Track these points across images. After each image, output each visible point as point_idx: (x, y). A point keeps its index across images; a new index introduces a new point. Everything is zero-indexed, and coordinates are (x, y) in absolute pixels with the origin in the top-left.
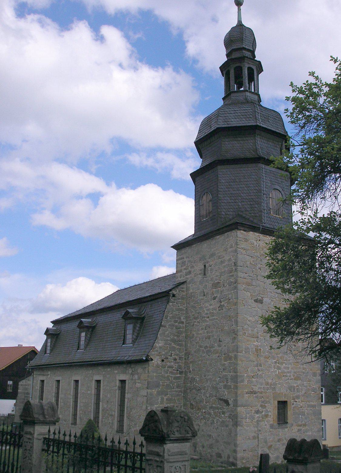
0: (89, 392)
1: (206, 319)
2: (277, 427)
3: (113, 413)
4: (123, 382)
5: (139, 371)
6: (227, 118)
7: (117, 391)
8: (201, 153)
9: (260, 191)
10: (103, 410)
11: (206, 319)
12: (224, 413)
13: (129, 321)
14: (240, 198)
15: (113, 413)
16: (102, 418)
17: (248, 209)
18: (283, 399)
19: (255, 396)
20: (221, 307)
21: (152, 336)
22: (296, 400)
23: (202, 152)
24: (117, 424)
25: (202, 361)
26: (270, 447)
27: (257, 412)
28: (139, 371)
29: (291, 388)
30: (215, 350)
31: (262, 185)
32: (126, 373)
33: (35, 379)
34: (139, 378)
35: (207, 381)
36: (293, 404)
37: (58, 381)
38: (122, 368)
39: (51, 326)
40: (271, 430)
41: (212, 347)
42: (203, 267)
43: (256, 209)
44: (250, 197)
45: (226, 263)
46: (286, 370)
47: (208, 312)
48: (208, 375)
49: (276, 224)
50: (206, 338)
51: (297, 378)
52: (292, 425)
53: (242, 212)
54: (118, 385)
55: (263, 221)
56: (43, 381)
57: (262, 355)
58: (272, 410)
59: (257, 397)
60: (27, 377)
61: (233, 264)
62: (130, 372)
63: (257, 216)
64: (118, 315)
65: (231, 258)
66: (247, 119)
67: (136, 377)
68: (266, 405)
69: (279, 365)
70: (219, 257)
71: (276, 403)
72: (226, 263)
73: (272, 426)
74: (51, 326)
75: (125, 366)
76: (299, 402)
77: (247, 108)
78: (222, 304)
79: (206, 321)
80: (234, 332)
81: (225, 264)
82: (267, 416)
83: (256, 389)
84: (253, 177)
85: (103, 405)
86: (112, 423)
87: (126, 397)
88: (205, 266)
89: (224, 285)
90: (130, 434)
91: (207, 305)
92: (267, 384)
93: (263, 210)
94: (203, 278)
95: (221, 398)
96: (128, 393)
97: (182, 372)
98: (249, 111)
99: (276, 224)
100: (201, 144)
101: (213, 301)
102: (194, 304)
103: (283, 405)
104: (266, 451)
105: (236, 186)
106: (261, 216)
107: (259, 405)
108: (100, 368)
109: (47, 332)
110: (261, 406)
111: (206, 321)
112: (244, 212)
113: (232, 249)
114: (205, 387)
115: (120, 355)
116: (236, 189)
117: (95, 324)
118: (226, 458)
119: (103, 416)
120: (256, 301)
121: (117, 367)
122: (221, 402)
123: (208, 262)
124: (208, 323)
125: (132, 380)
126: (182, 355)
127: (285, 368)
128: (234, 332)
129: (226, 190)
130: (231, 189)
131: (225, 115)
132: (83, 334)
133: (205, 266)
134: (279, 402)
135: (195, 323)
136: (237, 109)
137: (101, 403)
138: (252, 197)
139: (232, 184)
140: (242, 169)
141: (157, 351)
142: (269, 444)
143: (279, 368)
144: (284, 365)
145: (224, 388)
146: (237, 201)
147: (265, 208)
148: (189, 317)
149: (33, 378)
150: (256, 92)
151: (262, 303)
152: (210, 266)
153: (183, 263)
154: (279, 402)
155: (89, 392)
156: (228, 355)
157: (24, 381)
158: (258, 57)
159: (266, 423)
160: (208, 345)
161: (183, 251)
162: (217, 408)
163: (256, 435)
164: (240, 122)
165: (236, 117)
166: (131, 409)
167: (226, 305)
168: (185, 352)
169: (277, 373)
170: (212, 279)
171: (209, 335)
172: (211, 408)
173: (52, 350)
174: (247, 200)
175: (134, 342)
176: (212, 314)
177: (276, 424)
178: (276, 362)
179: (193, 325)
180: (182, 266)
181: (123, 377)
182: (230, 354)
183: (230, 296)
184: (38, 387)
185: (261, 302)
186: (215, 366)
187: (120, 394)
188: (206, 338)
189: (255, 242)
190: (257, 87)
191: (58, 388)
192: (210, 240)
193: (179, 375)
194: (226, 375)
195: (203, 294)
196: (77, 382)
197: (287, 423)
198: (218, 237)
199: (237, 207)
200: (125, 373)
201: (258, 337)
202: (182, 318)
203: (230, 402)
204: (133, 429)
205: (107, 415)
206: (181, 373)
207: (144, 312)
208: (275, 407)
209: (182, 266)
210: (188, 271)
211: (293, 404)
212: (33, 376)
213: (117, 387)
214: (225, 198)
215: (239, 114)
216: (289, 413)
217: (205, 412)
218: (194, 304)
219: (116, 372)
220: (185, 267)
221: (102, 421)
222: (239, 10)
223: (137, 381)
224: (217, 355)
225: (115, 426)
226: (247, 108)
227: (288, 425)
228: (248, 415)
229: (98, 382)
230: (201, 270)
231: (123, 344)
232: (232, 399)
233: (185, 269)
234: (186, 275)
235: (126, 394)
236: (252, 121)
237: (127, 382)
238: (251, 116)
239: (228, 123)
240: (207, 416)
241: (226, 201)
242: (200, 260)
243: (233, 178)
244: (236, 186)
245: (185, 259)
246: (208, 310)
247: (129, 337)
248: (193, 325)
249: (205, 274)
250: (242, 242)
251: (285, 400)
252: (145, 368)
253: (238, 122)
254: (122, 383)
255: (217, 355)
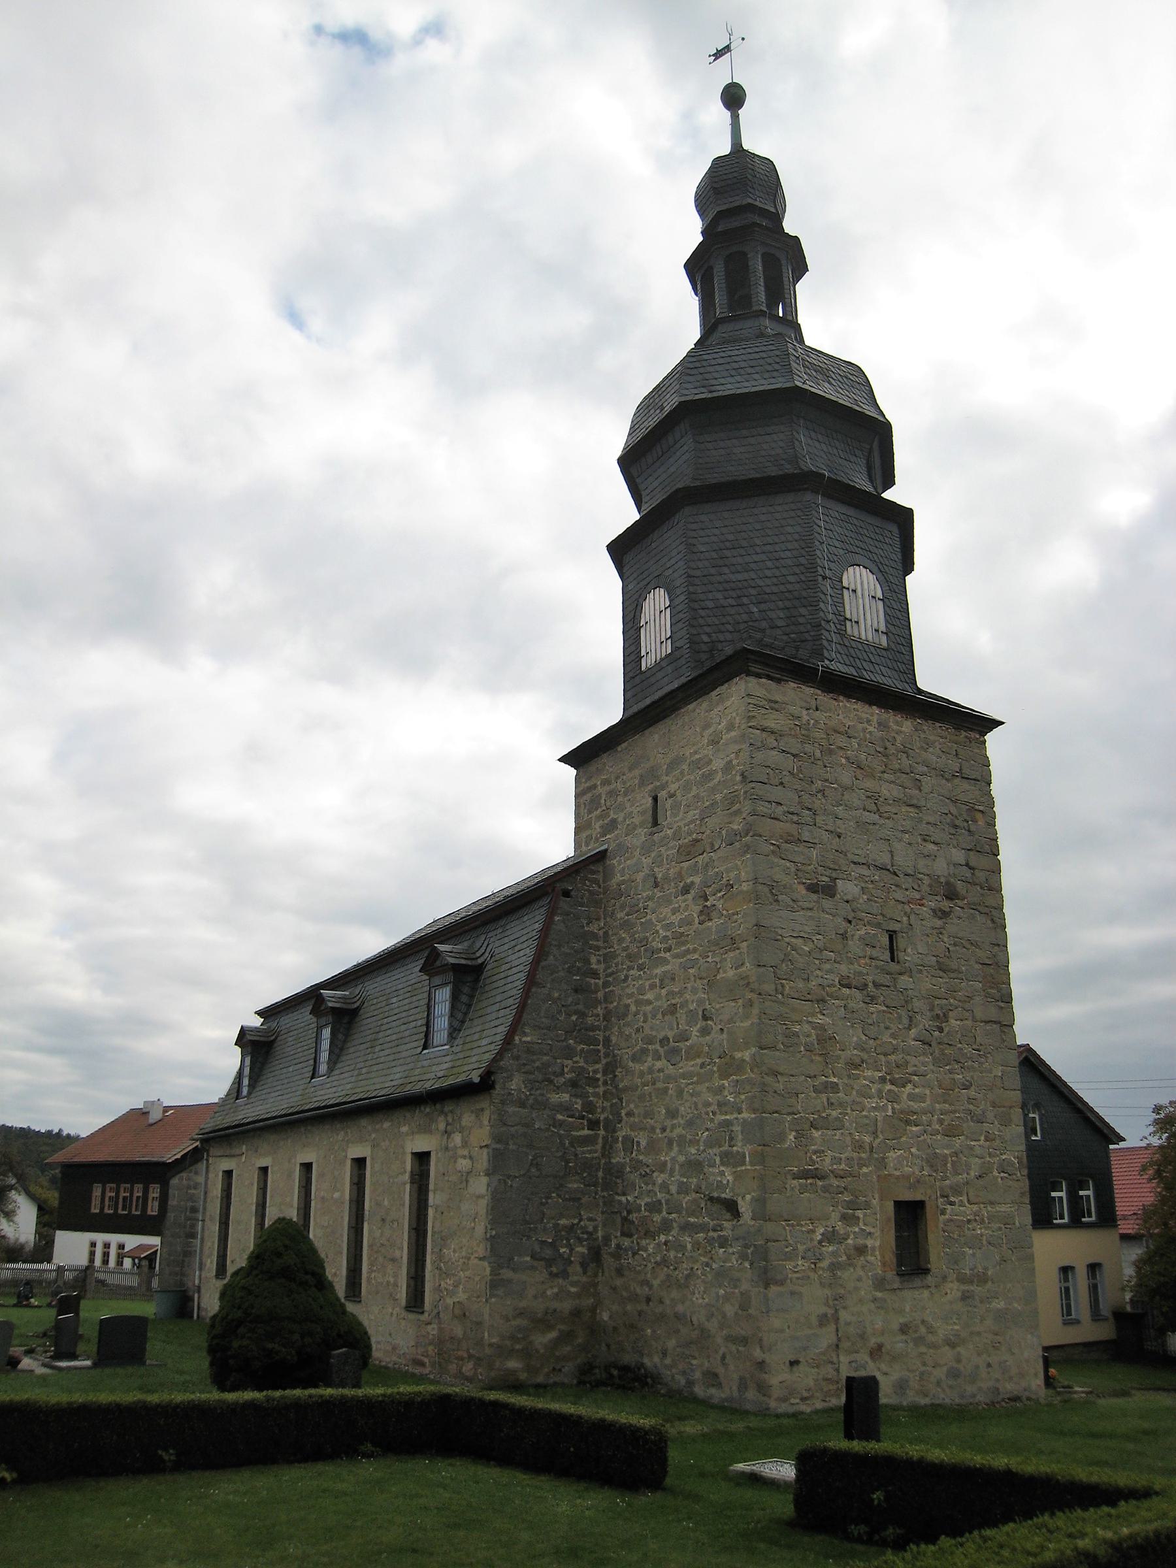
0: (337, 1195)
2: (896, 1286)
4: (422, 1158)
5: (464, 1123)
6: (707, 376)
7: (408, 1187)
8: (640, 496)
9: (812, 567)
10: (371, 1246)
12: (723, 1243)
13: (437, 980)
14: (753, 592)
15: (397, 1253)
16: (371, 1271)
17: (780, 623)
18: (908, 1196)
19: (823, 1186)
20: (706, 913)
21: (502, 1013)
22: (952, 1199)
23: (642, 487)
24: (408, 1286)
25: (654, 1084)
26: (877, 1352)
27: (831, 1237)
28: (464, 1123)
29: (934, 1162)
30: (691, 1047)
31: (818, 552)
32: (431, 1132)
33: (211, 1168)
34: (465, 1144)
35: (670, 1143)
36: (943, 1212)
38: (418, 1116)
40: (879, 1295)
43: (801, 620)
44: (782, 588)
45: (719, 777)
46: (915, 1106)
47: (668, 934)
49: (864, 664)
51: (951, 1132)
52: (944, 1278)
53: (763, 631)
54: (409, 1168)
55: (826, 654)
56: (228, 1174)
57: (839, 1057)
58: (877, 1234)
59: (826, 1189)
60: (191, 1165)
61: (738, 778)
62: (442, 1126)
63: (806, 640)
64: (412, 972)
65: (731, 761)
66: (766, 375)
67: (457, 1139)
68: (859, 1213)
69: (893, 1087)
70: (697, 765)
71: (890, 1206)
72: (719, 777)
73: (880, 1284)
74: (257, 1022)
75: (428, 1110)
76: (962, 1204)
77: (764, 348)
78: (708, 903)
80: (748, 984)
81: (716, 781)
82: (861, 1250)
83: (826, 1164)
84: (789, 529)
85: (370, 1231)
86: (396, 1285)
87: (431, 1201)
88: (655, 799)
89: (712, 845)
90: (441, 1315)
91: (666, 911)
92: (859, 1146)
93: (823, 623)
96: (435, 1191)
97: (597, 1122)
98: (771, 354)
99: (864, 664)
100: (633, 462)
102: (627, 915)
103: (910, 1215)
104: (871, 1369)
105: (740, 560)
106: (818, 638)
107: (835, 1216)
108: (364, 1122)
109: (244, 1038)
110: (844, 1217)
111: (665, 961)
112: (768, 632)
113: (733, 734)
114: (665, 1163)
115: (412, 1079)
116: (739, 568)
117: (358, 1004)
118: (735, 1388)
119: (371, 1264)
120: (813, 888)
121: (408, 1115)
122: (716, 1208)
123: (663, 787)
124: (669, 967)
125: (447, 1148)
127: (912, 1097)
128: (748, 984)
129: (713, 571)
130: (726, 570)
131: (702, 370)
132: (327, 1033)
133: (655, 799)
134: (898, 1204)
135: (632, 972)
136: (737, 352)
138: (790, 587)
139: (727, 553)
140: (756, 511)
141: (517, 1058)
142: (873, 1341)
143: (893, 1098)
144: (910, 1086)
146: (745, 600)
147: (831, 617)
148: (613, 956)
149: (207, 1167)
150: (790, 318)
151: (833, 896)
152: (671, 797)
153: (594, 803)
154: (898, 1204)
155: (337, 1195)
156: (732, 1057)
158: (790, 226)
159: (862, 1273)
160: (670, 1034)
161: (593, 766)
162: (702, 1228)
163: (830, 1312)
164: (746, 384)
165: (733, 373)
168: (604, 1061)
169: (890, 1113)
171: (673, 1002)
172: (686, 1227)
173: (252, 1086)
174: (773, 597)
176: (680, 938)
177: (891, 1275)
178: (883, 1080)
179: (627, 977)
181: (421, 1144)
182: (738, 1055)
183: (732, 875)
184: (216, 1190)
185: (829, 891)
186: (692, 1095)
187: (416, 1195)
188: (664, 1015)
189: (805, 712)
190: (791, 309)
191: (263, 1189)
192: (668, 721)
194: (728, 1123)
195: (652, 884)
197: (926, 1271)
198: (691, 707)
199: (745, 617)
201: (823, 1001)
202: (593, 959)
204: (450, 1301)
207: (482, 950)
208: (889, 1220)
209: (590, 812)
211: (943, 1212)
212: (207, 1160)
213: (407, 1177)
214: (710, 596)
215: (743, 364)
216: (931, 1236)
221: (369, 1279)
222: (735, 119)
223: (461, 1152)
224: (699, 1061)
225: (402, 1295)
226: (764, 348)
227: (930, 1279)
228: (801, 1248)
229: (360, 1163)
230: (643, 813)
231: (425, 1047)
232: (748, 1197)
233: (598, 818)
235: (431, 1195)
236: (780, 379)
237: (433, 1155)
238: (777, 367)
239: (713, 388)
240: (672, 1254)
241: (710, 604)
242: (642, 784)
243: (731, 537)
244: (740, 560)
245: (600, 790)
246: (667, 927)
248: (627, 977)
249: (655, 823)
250: (763, 711)
251: (919, 1197)
252: (482, 1110)
253: (738, 385)
255: (699, 1061)
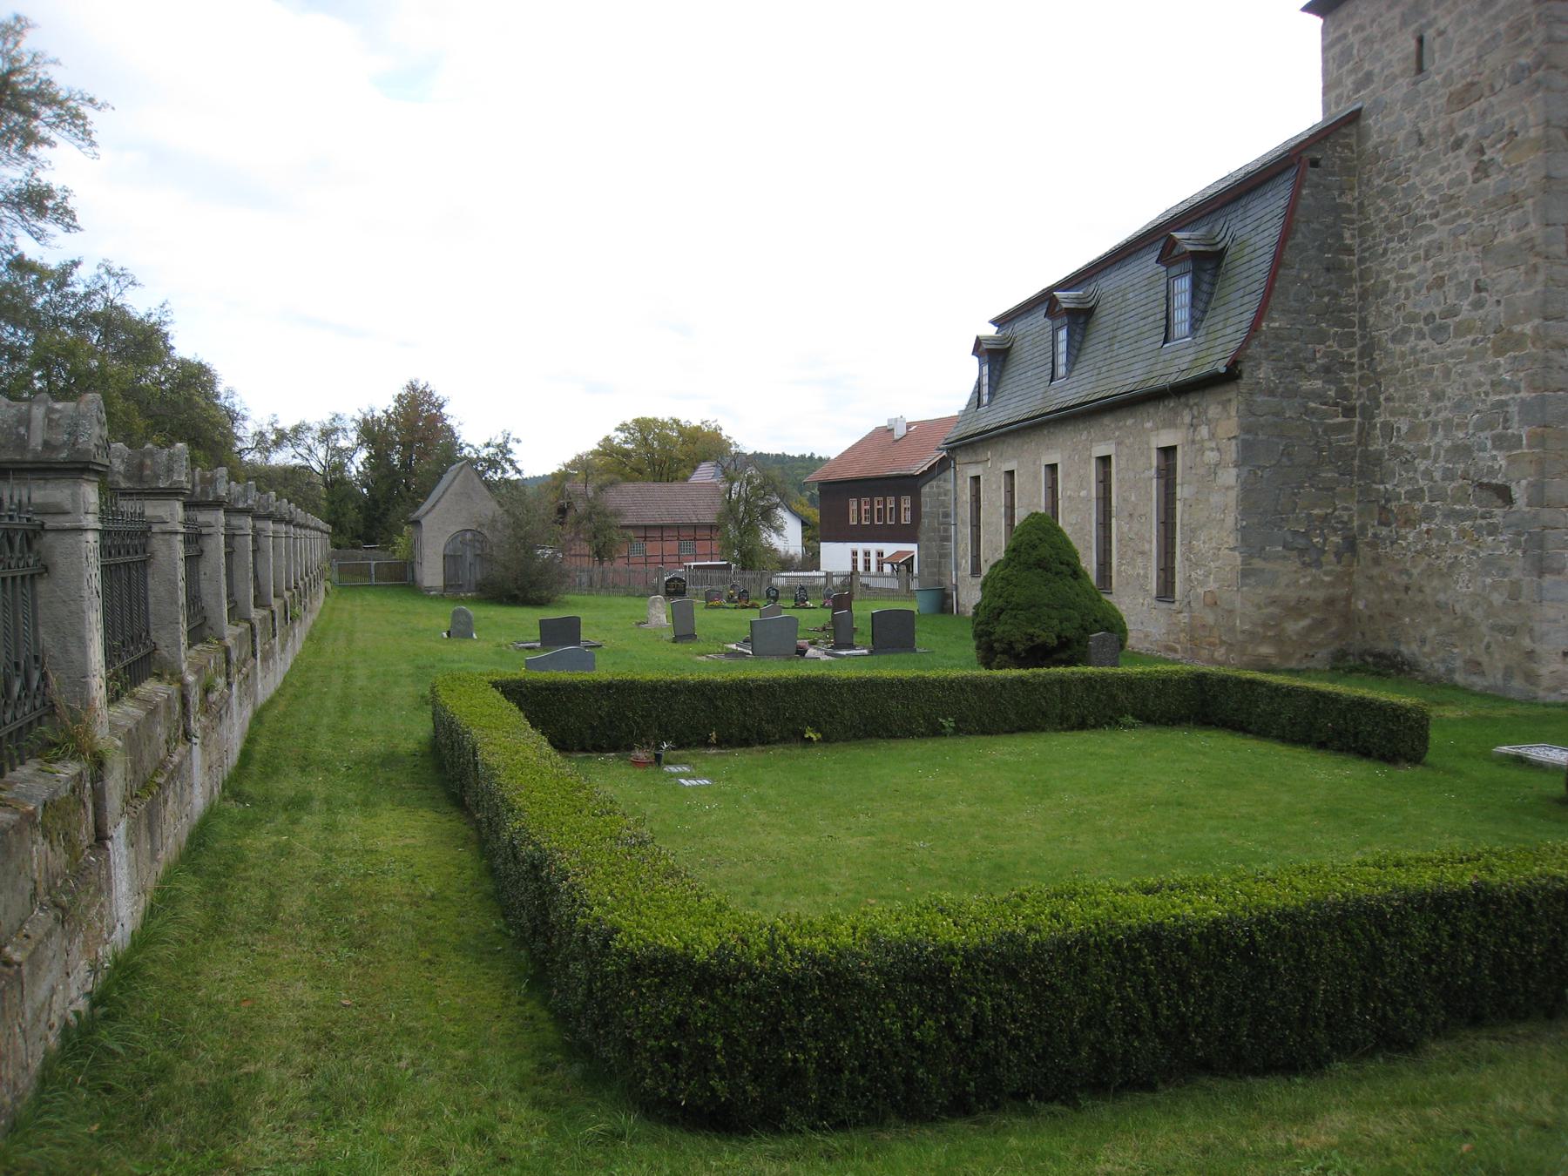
0: (1083, 493)
1: (1480, 510)
3: (1147, 546)
4: (1168, 452)
11: (1428, 222)
12: (1493, 530)
15: (1147, 546)
20: (1482, 170)
21: (1247, 299)
34: (1213, 436)
35: (1435, 427)
37: (1011, 473)
39: (992, 331)
41: (1452, 312)
42: (1413, 44)
47: (1436, 198)
48: (1439, 410)
50: (1429, 289)
54: (1155, 463)
56: (976, 479)
62: (1187, 419)
64: (1149, 263)
74: (992, 331)
78: (1485, 158)
79: (1431, 229)
80: (1533, 247)
87: (1178, 495)
88: (1420, 41)
89: (1492, 87)
91: (1432, 172)
94: (1416, 83)
95: (1485, 480)
101: (1450, 155)
102: (1387, 180)
108: (1107, 420)
111: (1431, 229)
121: (1151, 410)
122: (1485, 494)
123: (1430, 24)
124: (1436, 236)
125: (1193, 442)
126: (1350, 356)
128: (1533, 247)
133: (1420, 41)
135: (1392, 245)
137: (1113, 520)
145: (1495, 447)
155: (1083, 493)
156: (1510, 332)
157: (934, 483)
160: (1437, 310)
166: (1193, 531)
167: (1500, 158)
168: (1360, 344)
170: (1448, 80)
173: (992, 394)
175: (1194, 328)
179: (1385, 251)
180: (1340, 67)
181: (1166, 439)
184: (966, 496)
188: (1429, 289)
193: (1340, 419)
194: (1502, 404)
196: (1052, 468)
200: (1171, 425)
203: (1519, 493)
205: (1130, 553)
206: (1349, 411)
209: (1340, 67)
210: (1360, 75)
213: (1154, 471)
217: (1428, 532)
218: (1387, 180)
219: (1148, 425)
220: (1350, 66)
221: (1119, 572)
223: (1207, 444)
224: (1470, 338)
225: (1153, 586)
229: (1105, 461)
232: (1524, 482)
234: (1357, 91)
235: (1178, 489)
247: (1181, 316)
248: (1385, 251)
249: (1420, 69)
254: (1167, 459)
255: (1470, 338)
